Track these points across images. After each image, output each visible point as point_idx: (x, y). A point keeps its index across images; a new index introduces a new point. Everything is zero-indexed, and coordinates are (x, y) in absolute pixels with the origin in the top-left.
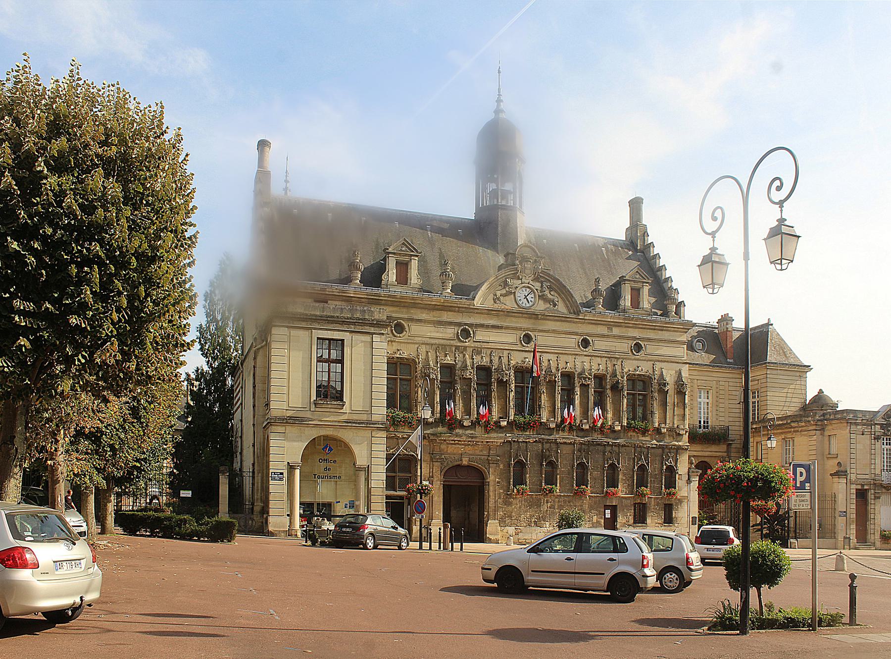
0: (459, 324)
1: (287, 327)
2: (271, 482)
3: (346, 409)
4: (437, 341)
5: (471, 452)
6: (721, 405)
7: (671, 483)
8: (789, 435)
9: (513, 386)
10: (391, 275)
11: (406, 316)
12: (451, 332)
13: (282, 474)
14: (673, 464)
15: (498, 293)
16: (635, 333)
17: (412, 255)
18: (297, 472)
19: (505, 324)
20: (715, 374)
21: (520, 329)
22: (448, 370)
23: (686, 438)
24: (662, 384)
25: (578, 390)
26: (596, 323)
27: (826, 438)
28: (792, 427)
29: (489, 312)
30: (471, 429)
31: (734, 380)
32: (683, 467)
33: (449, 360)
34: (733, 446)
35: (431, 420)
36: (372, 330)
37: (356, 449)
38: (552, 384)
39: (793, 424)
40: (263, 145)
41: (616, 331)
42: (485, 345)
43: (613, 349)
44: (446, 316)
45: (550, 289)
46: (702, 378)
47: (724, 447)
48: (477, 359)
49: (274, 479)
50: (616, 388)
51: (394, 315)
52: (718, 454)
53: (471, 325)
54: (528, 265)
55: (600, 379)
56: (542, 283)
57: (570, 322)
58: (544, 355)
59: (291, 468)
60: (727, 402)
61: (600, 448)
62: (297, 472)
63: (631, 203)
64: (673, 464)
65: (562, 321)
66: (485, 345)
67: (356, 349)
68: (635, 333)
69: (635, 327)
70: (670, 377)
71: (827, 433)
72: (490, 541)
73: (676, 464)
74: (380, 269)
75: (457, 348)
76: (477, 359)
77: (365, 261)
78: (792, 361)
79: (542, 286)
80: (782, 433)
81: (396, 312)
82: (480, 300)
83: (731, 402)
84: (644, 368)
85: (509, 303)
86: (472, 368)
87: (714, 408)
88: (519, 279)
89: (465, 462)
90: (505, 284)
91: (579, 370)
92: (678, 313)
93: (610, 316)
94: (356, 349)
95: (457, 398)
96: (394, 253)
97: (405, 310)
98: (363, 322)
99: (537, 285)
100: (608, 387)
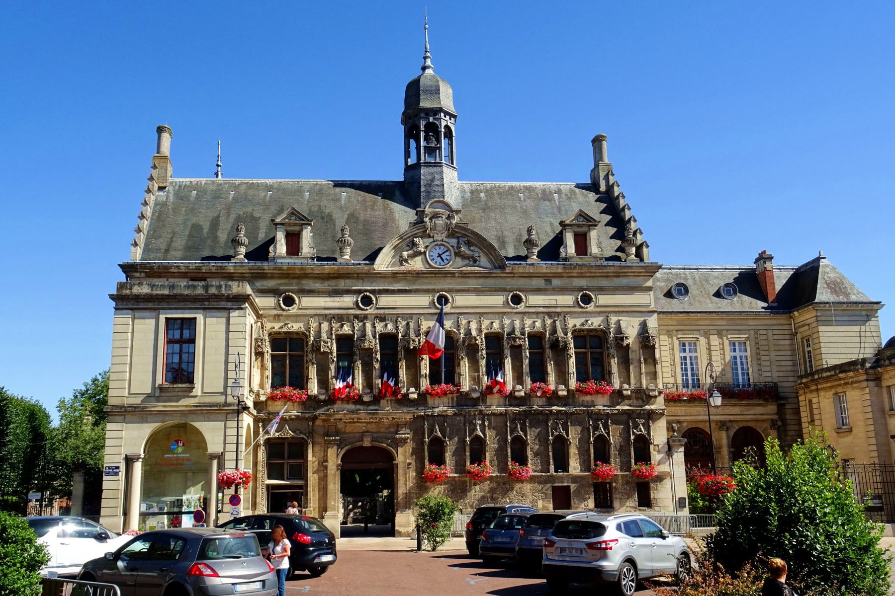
0: (359, 292)
1: (131, 309)
2: (105, 478)
3: (197, 390)
4: (332, 312)
5: (374, 430)
6: (763, 358)
7: (644, 456)
8: (840, 390)
9: (572, 352)
10: (570, 246)
11: (295, 288)
12: (348, 301)
13: (118, 468)
14: (644, 432)
15: (405, 254)
16: (583, 282)
17: (590, 226)
18: (138, 467)
19: (391, 288)
20: (750, 322)
21: (434, 291)
22: (345, 342)
23: (661, 400)
24: (620, 336)
25: (507, 352)
26: (530, 276)
27: (885, 391)
28: (840, 379)
29: (394, 276)
30: (375, 405)
31: (780, 327)
32: (659, 434)
33: (346, 329)
34: (788, 406)
35: (323, 397)
36: (229, 305)
37: (208, 437)
38: (517, 351)
39: (841, 375)
40: (597, 141)
41: (556, 282)
42: (387, 311)
43: (553, 303)
44: (342, 284)
45: (469, 244)
46: (733, 327)
47: (772, 408)
48: (380, 327)
49: (108, 474)
50: (559, 349)
51: (282, 288)
52: (765, 417)
53: (373, 292)
54: (439, 222)
55: (536, 339)
56: (458, 238)
57: (468, 277)
58: (462, 317)
59: (129, 461)
60: (773, 354)
61: (541, 417)
62: (138, 467)
63: (594, 141)
64: (644, 432)
65: (476, 277)
66: (387, 311)
67: (209, 328)
68: (583, 282)
69: (581, 276)
70: (631, 329)
71: (885, 383)
72: (400, 535)
73: (649, 433)
74: (558, 241)
75: (356, 317)
76: (380, 327)
77: (543, 238)
78: (853, 298)
79: (458, 243)
80: (832, 387)
81: (286, 284)
82: (384, 263)
83: (779, 353)
84: (596, 322)
85: (417, 264)
86: (375, 337)
87: (755, 363)
88: (429, 236)
89: (367, 443)
90: (413, 245)
91: (507, 330)
92: (639, 255)
93: (546, 267)
94: (209, 328)
95: (356, 372)
96: (282, 224)
97: (295, 281)
98: (218, 297)
99: (454, 241)
100: (547, 346)
